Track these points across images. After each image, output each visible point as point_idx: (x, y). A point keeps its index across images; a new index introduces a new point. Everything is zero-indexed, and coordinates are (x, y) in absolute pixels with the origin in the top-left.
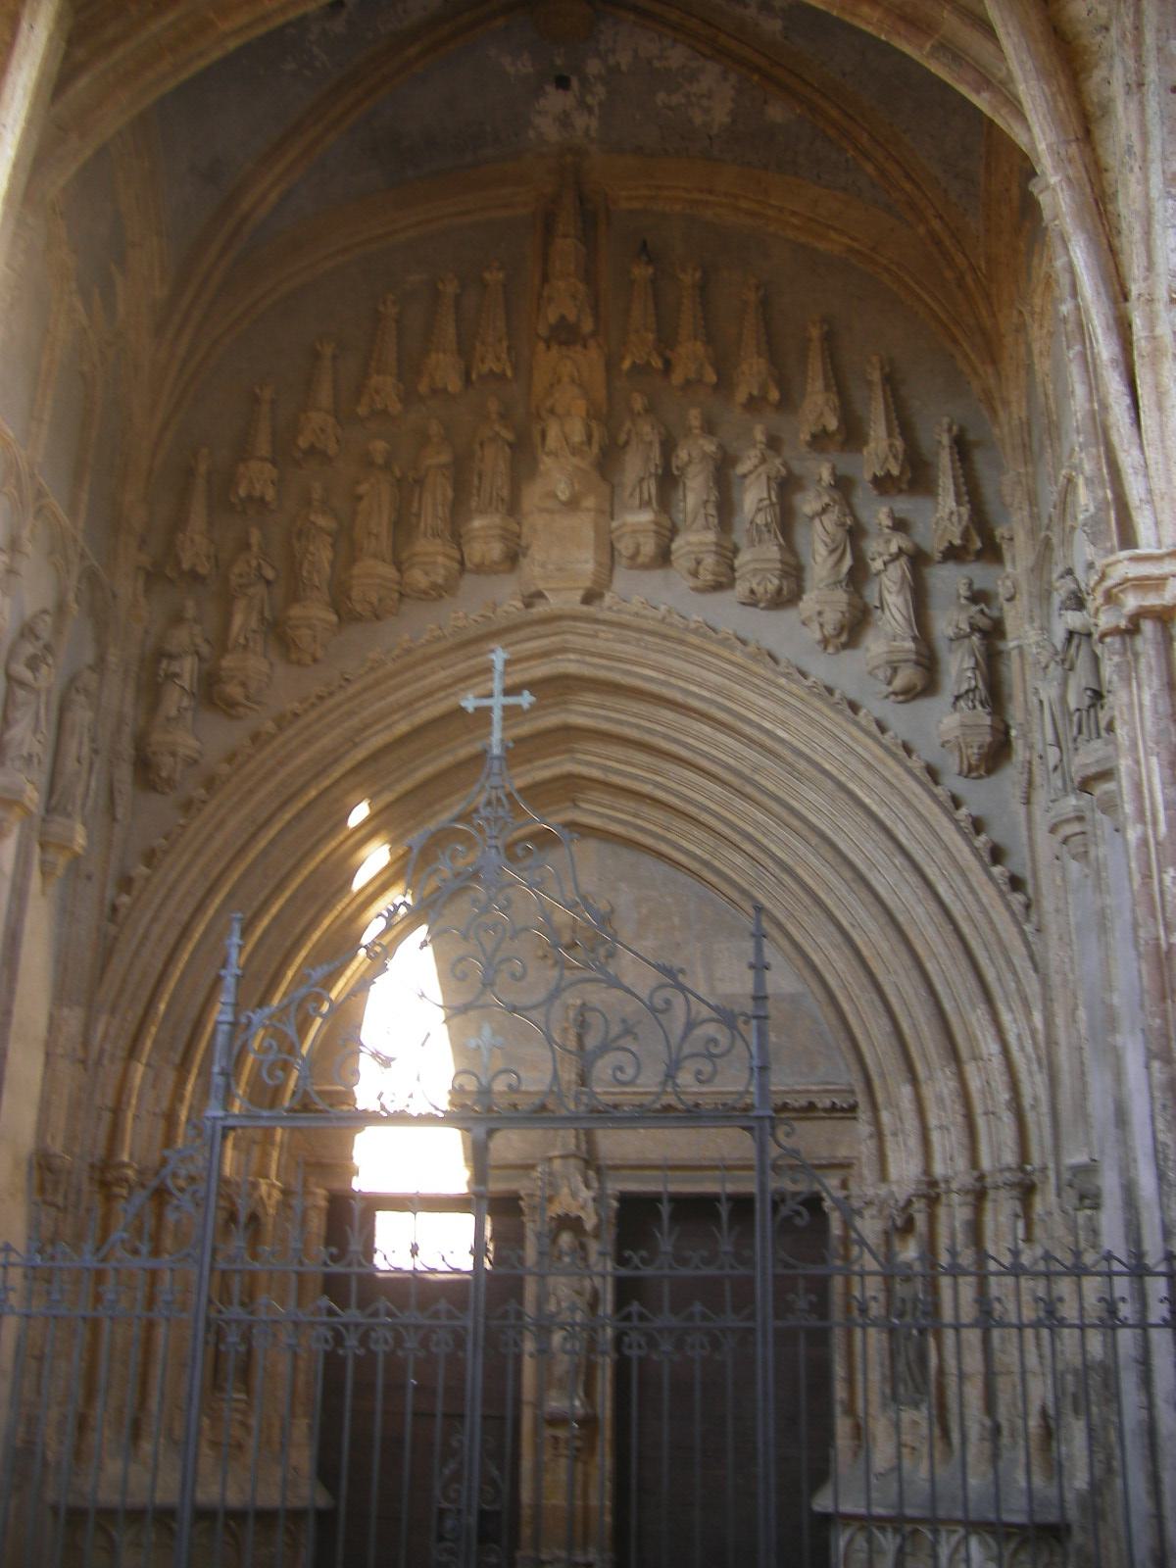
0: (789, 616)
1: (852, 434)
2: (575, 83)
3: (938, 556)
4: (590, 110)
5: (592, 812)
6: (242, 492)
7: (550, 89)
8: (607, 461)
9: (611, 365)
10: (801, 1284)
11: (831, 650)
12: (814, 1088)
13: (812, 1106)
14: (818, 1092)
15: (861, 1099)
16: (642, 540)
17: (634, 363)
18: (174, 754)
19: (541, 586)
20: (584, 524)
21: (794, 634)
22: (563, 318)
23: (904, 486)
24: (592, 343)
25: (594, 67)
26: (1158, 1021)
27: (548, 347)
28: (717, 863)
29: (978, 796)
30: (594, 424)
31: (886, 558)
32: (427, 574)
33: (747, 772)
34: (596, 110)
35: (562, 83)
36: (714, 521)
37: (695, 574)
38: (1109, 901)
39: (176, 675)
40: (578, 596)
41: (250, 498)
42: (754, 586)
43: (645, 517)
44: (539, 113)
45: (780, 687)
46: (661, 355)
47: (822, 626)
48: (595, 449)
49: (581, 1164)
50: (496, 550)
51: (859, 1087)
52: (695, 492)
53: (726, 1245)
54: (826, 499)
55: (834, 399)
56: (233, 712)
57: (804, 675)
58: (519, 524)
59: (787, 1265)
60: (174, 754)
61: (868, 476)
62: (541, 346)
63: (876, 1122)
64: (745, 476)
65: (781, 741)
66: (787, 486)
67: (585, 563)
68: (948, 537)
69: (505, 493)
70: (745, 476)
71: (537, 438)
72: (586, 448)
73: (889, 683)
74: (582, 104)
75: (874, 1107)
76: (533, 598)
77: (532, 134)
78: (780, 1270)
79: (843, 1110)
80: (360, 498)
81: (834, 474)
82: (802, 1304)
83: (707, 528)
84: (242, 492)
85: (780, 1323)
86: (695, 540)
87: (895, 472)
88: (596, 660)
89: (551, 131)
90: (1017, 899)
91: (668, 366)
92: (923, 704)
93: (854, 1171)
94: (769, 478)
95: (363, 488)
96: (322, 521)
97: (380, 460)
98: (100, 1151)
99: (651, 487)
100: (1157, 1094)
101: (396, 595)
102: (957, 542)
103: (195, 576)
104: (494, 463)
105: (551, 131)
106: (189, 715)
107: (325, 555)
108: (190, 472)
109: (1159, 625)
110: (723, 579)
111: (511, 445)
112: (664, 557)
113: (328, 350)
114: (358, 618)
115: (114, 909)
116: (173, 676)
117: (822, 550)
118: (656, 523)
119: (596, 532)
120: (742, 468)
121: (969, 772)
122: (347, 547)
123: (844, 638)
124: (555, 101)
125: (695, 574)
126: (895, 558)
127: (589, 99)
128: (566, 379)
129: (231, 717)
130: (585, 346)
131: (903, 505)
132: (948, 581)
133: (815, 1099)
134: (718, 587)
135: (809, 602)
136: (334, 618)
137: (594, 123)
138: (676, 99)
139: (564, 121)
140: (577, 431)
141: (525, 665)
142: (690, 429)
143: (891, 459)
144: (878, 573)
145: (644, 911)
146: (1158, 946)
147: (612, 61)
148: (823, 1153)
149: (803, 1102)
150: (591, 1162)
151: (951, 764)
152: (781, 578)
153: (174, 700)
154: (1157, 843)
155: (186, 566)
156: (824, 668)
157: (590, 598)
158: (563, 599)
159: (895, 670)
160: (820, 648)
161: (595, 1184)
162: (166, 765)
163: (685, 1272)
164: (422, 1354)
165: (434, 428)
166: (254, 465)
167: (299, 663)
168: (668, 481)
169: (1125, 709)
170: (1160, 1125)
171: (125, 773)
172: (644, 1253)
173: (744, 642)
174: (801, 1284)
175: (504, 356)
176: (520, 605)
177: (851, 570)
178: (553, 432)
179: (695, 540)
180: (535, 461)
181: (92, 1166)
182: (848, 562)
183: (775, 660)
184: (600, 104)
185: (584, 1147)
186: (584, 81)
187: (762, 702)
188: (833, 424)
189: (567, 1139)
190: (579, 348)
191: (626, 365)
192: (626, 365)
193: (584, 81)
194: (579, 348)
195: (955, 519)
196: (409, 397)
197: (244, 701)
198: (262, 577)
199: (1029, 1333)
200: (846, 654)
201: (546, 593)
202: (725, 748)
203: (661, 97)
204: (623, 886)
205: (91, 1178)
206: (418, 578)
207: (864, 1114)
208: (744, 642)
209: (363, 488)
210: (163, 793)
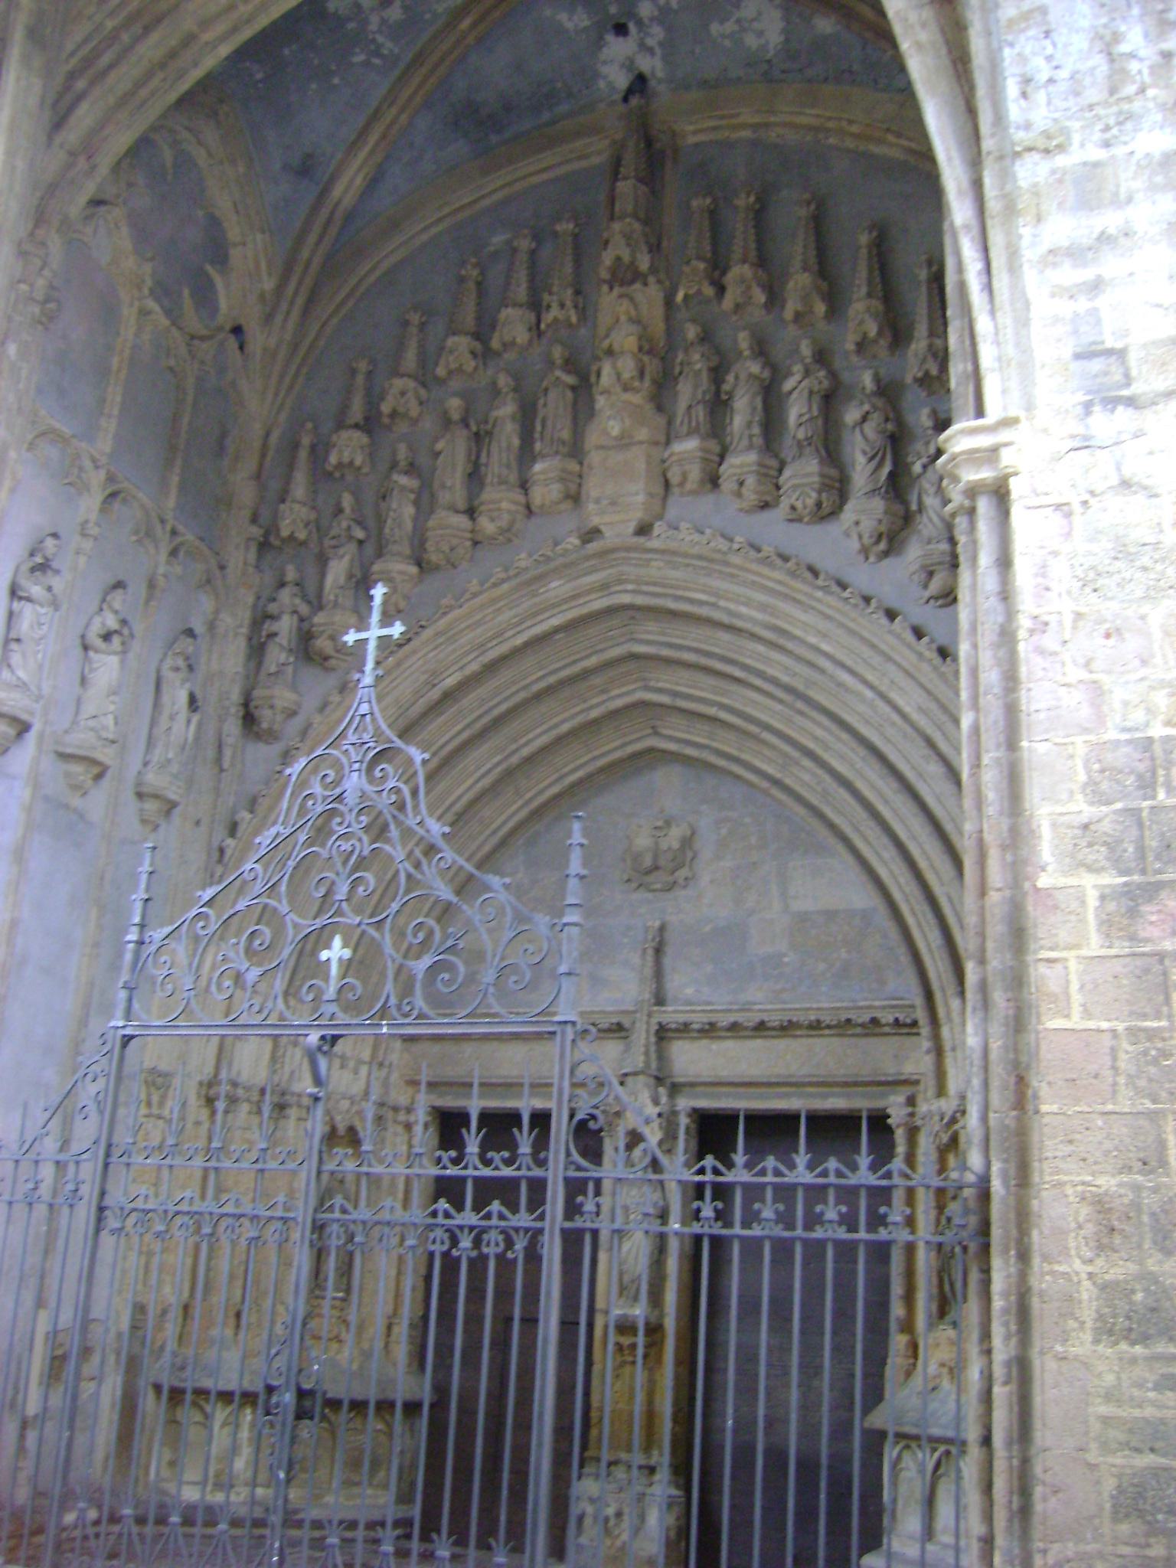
0: (833, 530)
4: (651, 51)
5: (675, 734)
7: (610, 38)
10: (769, 1193)
11: (872, 559)
12: (877, 1003)
13: (874, 1021)
14: (884, 1007)
15: (921, 1015)
16: (687, 467)
18: (272, 707)
19: (596, 521)
21: (837, 544)
22: (618, 259)
24: (651, 279)
27: (611, 288)
28: (788, 781)
30: (646, 359)
31: (924, 460)
32: (492, 520)
33: (801, 687)
34: (658, 51)
35: (621, 30)
36: (758, 441)
37: (739, 495)
39: (275, 634)
40: (631, 527)
45: (819, 601)
46: (713, 283)
47: (860, 537)
48: (647, 383)
49: (652, 1081)
50: (555, 491)
51: (919, 1001)
52: (743, 411)
53: (525, 1148)
54: (866, 407)
55: (877, 305)
57: (844, 586)
58: (581, 463)
59: (579, 1168)
60: (272, 707)
62: (605, 288)
63: (936, 1037)
64: (790, 393)
65: (826, 655)
66: (830, 400)
67: (637, 496)
69: (566, 435)
70: (790, 393)
72: (637, 384)
73: (926, 587)
74: (642, 46)
75: (934, 1021)
76: (593, 534)
77: (602, 84)
78: (572, 1173)
79: (905, 1025)
80: (438, 454)
81: (877, 379)
82: (831, 1214)
83: (751, 447)
85: (568, 1225)
86: (742, 462)
88: (651, 589)
91: (721, 290)
93: (921, 1087)
94: (811, 393)
95: (439, 446)
96: (403, 480)
97: (456, 416)
98: (209, 1070)
99: (700, 413)
101: (468, 544)
104: (555, 407)
106: (290, 669)
107: (409, 511)
108: (296, 446)
109: (994, 500)
110: (768, 498)
111: (573, 388)
112: (713, 481)
113: (415, 318)
114: (437, 568)
115: (222, 851)
116: (272, 635)
117: (861, 460)
118: (702, 450)
119: (648, 463)
120: (788, 385)
122: (425, 501)
123: (883, 546)
124: (617, 48)
125: (739, 495)
127: (649, 42)
128: (623, 318)
129: (327, 670)
130: (646, 284)
133: (878, 1014)
134: (765, 506)
135: (849, 514)
136: (414, 570)
138: (730, 27)
140: (627, 366)
142: (741, 353)
143: (930, 359)
144: (919, 476)
145: (724, 831)
148: (890, 1069)
149: (865, 1017)
150: (663, 1080)
152: (819, 492)
153: (276, 656)
156: (864, 576)
157: (643, 530)
158: (617, 528)
159: (931, 574)
160: (861, 558)
161: (664, 1099)
162: (266, 718)
163: (487, 1172)
164: (474, 1253)
165: (503, 380)
168: (719, 405)
171: (233, 728)
172: (506, 1154)
173: (786, 559)
174: (769, 1193)
175: (569, 303)
176: (577, 542)
177: (892, 475)
178: (607, 370)
179: (742, 462)
180: (591, 401)
181: (201, 1084)
182: (887, 469)
183: (815, 573)
185: (654, 1065)
186: (640, 23)
187: (803, 617)
189: (638, 1052)
190: (637, 286)
198: (351, 538)
200: (886, 562)
201: (603, 528)
202: (778, 666)
203: (715, 28)
204: (704, 807)
205: (199, 1094)
206: (487, 526)
207: (925, 1030)
208: (786, 559)
209: (439, 446)
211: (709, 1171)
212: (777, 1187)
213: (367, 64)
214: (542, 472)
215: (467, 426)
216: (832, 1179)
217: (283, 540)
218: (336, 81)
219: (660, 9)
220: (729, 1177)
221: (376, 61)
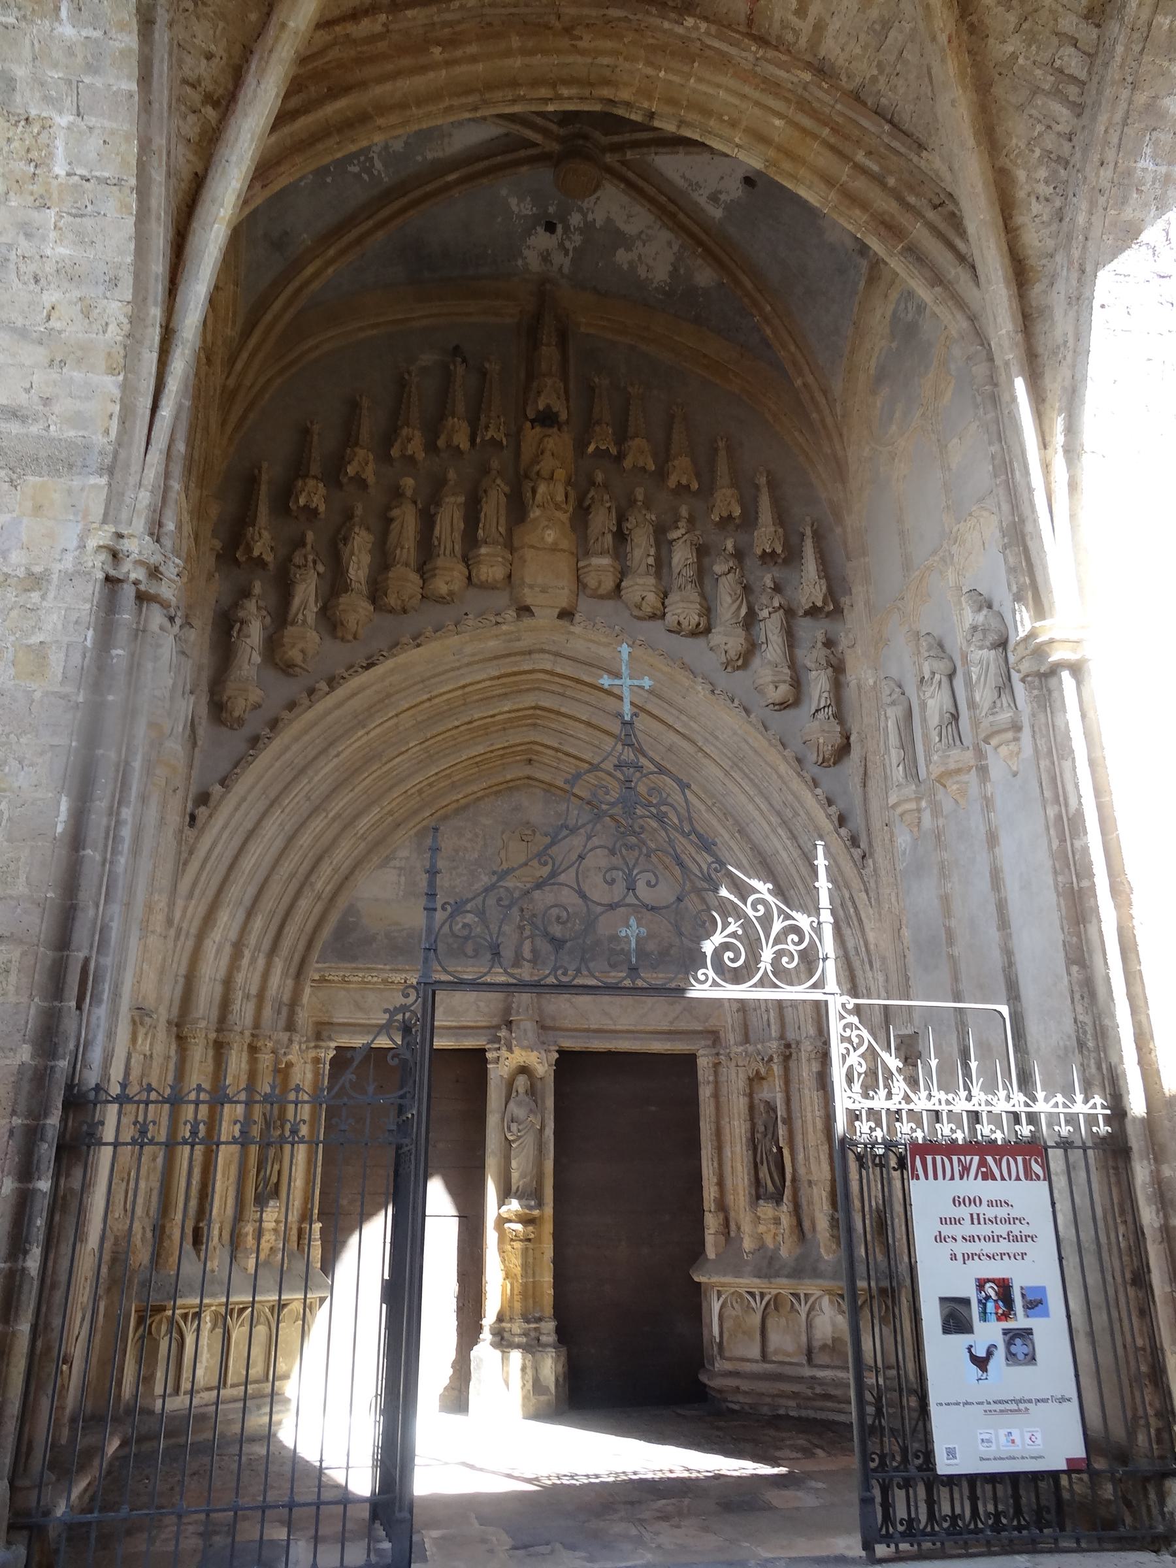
0: (700, 642)
1: (749, 521)
2: (559, 228)
3: (801, 613)
6: (302, 501)
7: (540, 230)
8: (581, 515)
9: (580, 446)
11: (729, 669)
17: (597, 447)
20: (564, 564)
23: (780, 561)
24: (565, 428)
25: (575, 219)
26: (1075, 939)
29: (828, 777)
30: (569, 488)
35: (550, 228)
38: (946, 856)
41: (306, 507)
42: (681, 619)
43: (605, 561)
44: (529, 247)
56: (291, 670)
61: (759, 552)
62: (528, 424)
66: (702, 551)
68: (813, 599)
71: (529, 494)
72: (564, 506)
74: (561, 245)
77: (520, 262)
81: (735, 546)
83: (648, 573)
84: (302, 501)
87: (779, 551)
89: (535, 264)
90: (857, 853)
92: (790, 713)
100: (1076, 988)
102: (819, 604)
103: (260, 563)
105: (535, 264)
110: (658, 613)
121: (823, 763)
124: (542, 240)
126: (776, 610)
127: (567, 244)
129: (288, 675)
131: (777, 572)
132: (811, 632)
135: (716, 637)
137: (567, 262)
139: (546, 257)
141: (518, 658)
142: (635, 501)
144: (765, 619)
146: (1073, 888)
147: (590, 217)
151: (812, 757)
152: (699, 615)
154: (1069, 819)
155: (256, 553)
156: (724, 680)
166: (311, 483)
167: (343, 639)
169: (1043, 728)
170: (1079, 1009)
178: (542, 489)
182: (744, 611)
184: (575, 249)
186: (567, 229)
188: (737, 512)
190: (555, 429)
191: (591, 448)
192: (591, 448)
193: (567, 229)
194: (555, 429)
195: (817, 586)
196: (431, 447)
197: (300, 664)
199: (115, 1090)
206: (441, 586)
210: (232, 728)
211: (1060, 1105)
212: (1029, 1115)
213: (357, 176)
214: (487, 555)
215: (415, 503)
216: (1061, 1109)
217: (250, 559)
218: (329, 180)
219: (586, 223)
220: (1035, 1108)
221: (365, 177)
